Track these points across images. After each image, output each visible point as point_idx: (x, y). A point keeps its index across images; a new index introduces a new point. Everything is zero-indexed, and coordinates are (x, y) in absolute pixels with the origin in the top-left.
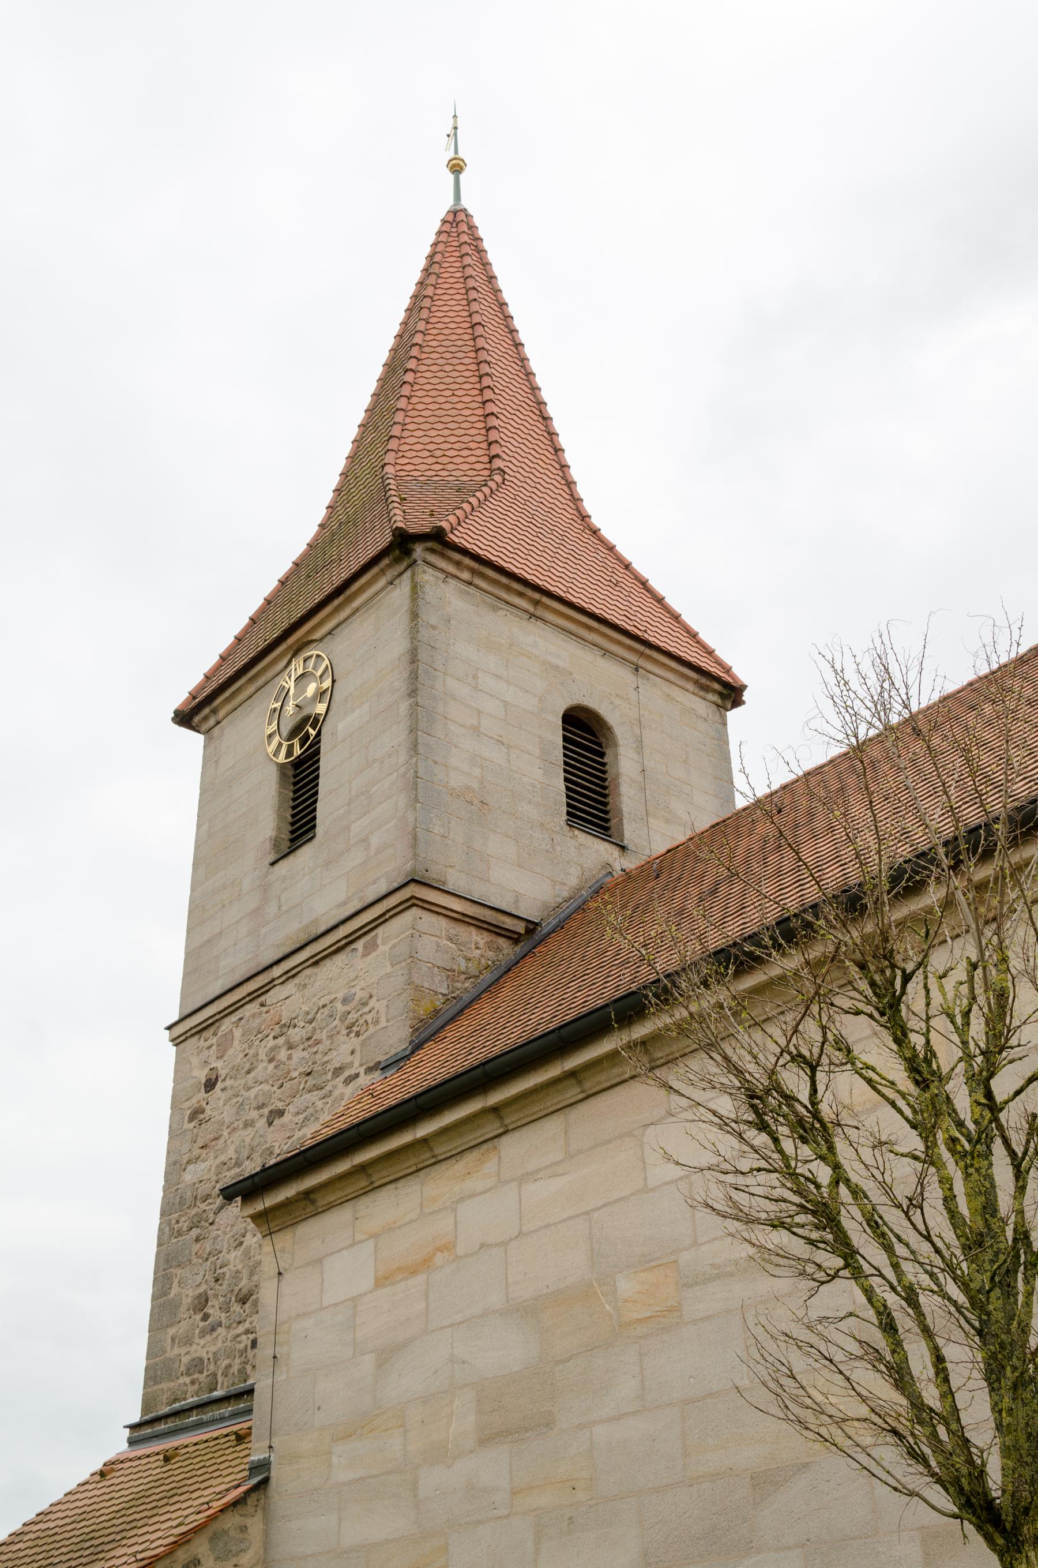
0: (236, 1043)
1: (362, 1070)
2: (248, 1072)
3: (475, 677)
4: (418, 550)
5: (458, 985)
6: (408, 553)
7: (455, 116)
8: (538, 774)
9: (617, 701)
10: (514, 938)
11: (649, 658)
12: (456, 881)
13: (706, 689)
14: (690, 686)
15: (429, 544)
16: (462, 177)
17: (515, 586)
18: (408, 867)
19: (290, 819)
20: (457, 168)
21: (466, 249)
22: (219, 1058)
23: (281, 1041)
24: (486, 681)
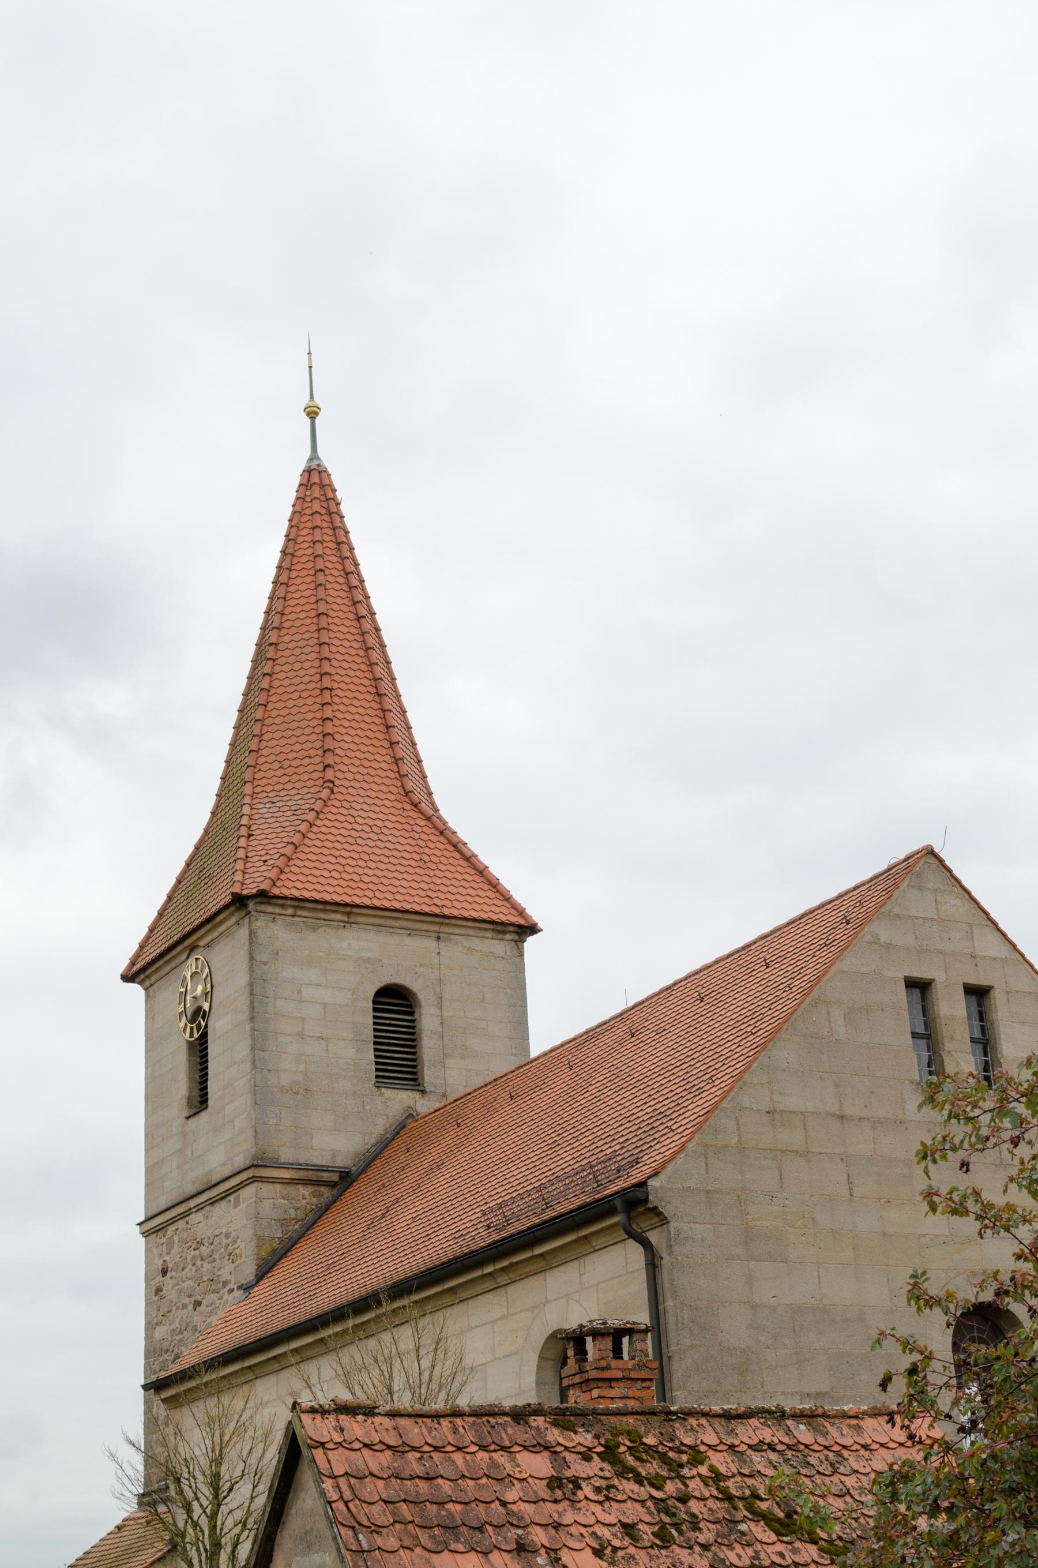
0: (176, 1246)
1: (235, 1287)
2: (183, 1269)
3: (299, 992)
4: (251, 905)
5: (290, 1228)
6: (245, 906)
7: (310, 353)
8: (351, 1052)
9: (421, 970)
10: (332, 1185)
11: (448, 924)
12: (287, 1155)
13: (504, 932)
14: (489, 934)
15: (258, 900)
16: (317, 420)
17: (329, 908)
18: (253, 1151)
19: (199, 1080)
20: (312, 413)
21: (318, 521)
22: (168, 1254)
23: (197, 1252)
24: (308, 993)
